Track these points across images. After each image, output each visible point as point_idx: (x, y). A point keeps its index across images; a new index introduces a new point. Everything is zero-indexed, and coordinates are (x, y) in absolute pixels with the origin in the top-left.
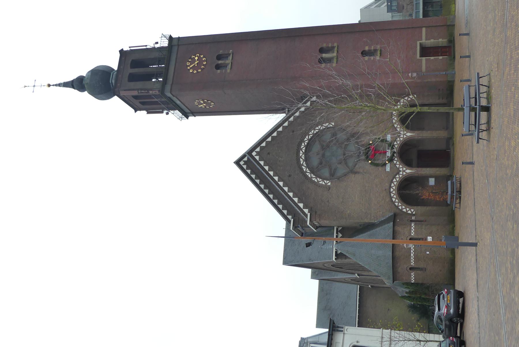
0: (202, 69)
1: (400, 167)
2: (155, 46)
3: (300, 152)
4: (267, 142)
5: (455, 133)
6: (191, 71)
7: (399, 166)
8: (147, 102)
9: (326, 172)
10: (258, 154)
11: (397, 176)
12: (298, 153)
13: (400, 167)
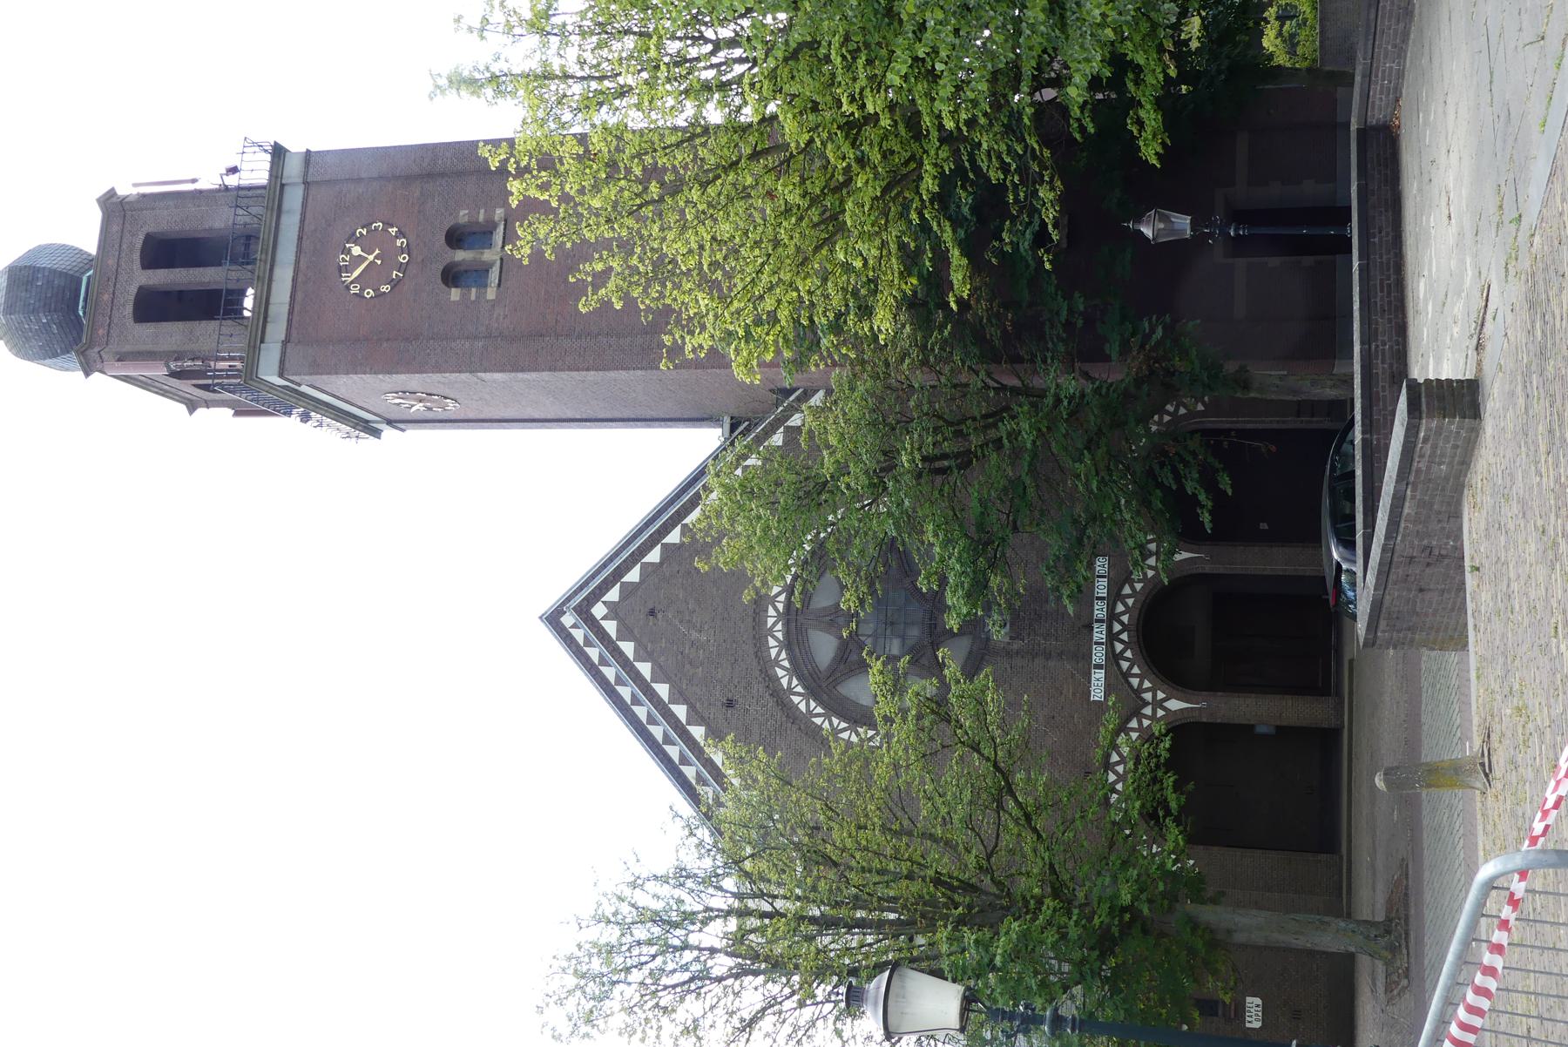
0: (395, 284)
1: (1144, 687)
2: (226, 183)
3: (767, 611)
4: (645, 566)
5: (1427, 839)
6: (354, 290)
10: (614, 611)
13: (1144, 687)
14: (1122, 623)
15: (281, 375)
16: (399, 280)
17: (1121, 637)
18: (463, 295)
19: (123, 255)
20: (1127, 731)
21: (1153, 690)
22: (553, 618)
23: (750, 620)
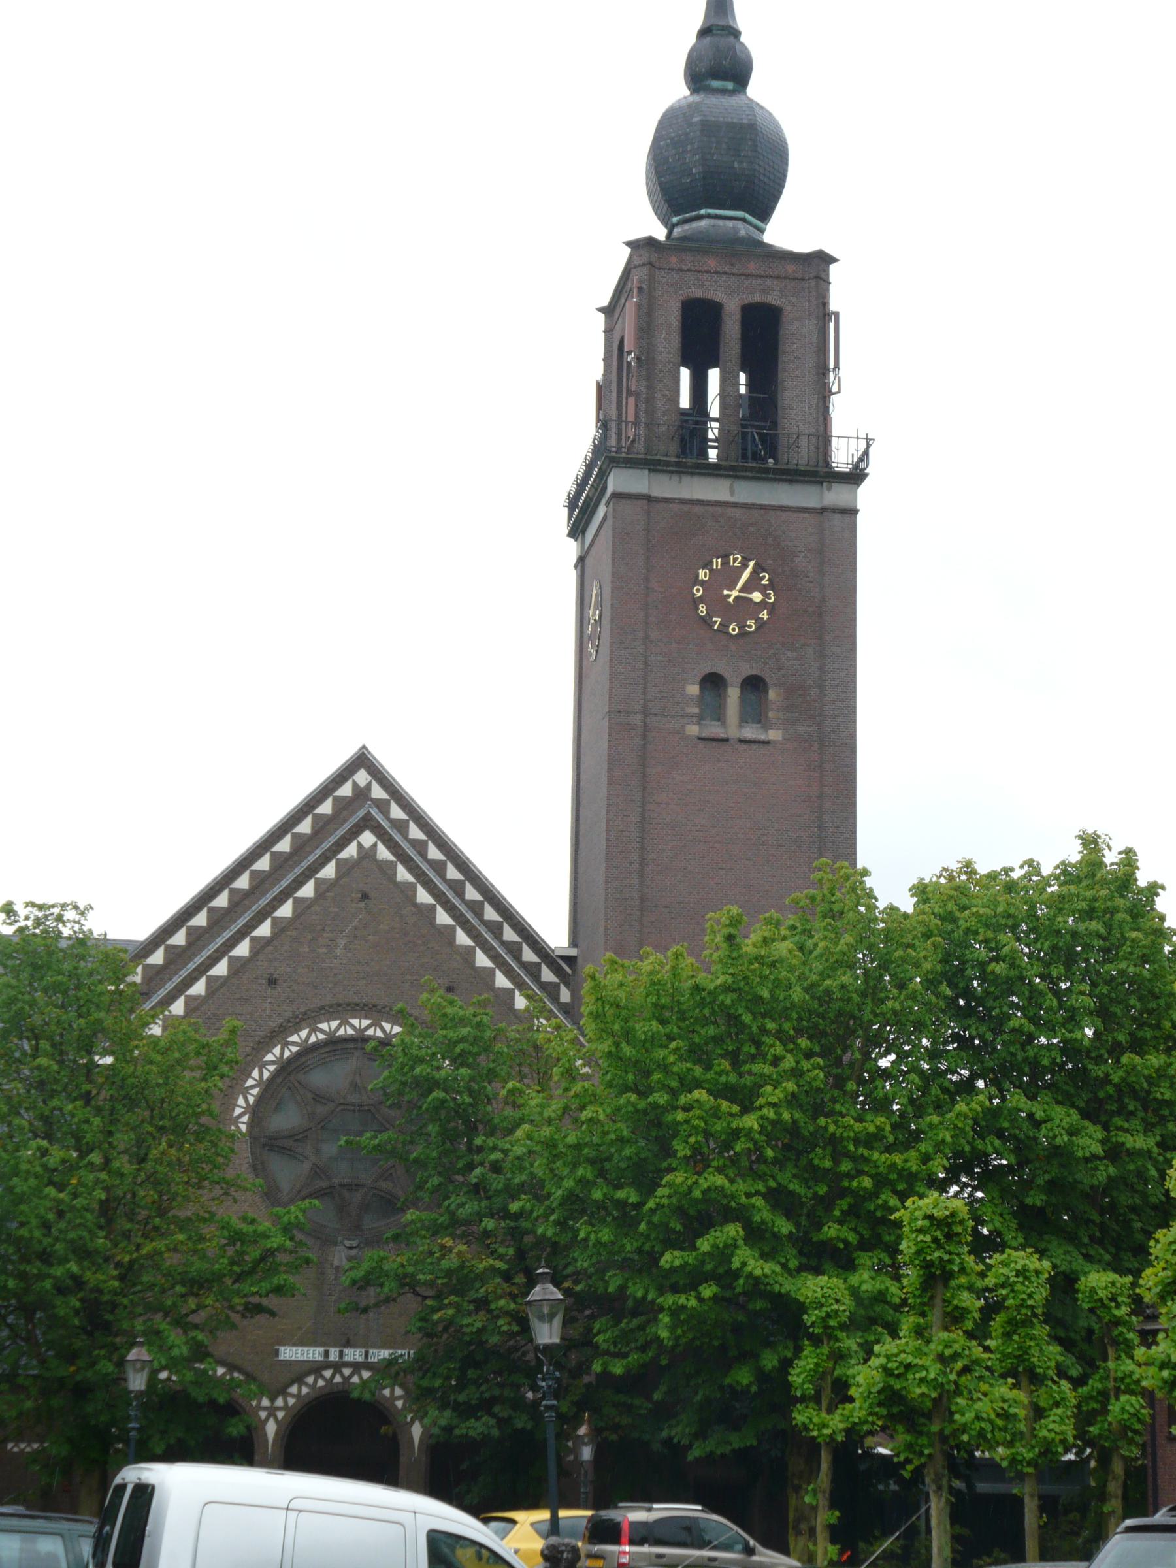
0: (706, 622)
7: (292, 1395)
9: (286, 1120)
10: (367, 855)
12: (362, 1009)
14: (351, 1376)
16: (710, 625)
18: (691, 698)
19: (760, 281)
21: (285, 1407)
23: (357, 1000)
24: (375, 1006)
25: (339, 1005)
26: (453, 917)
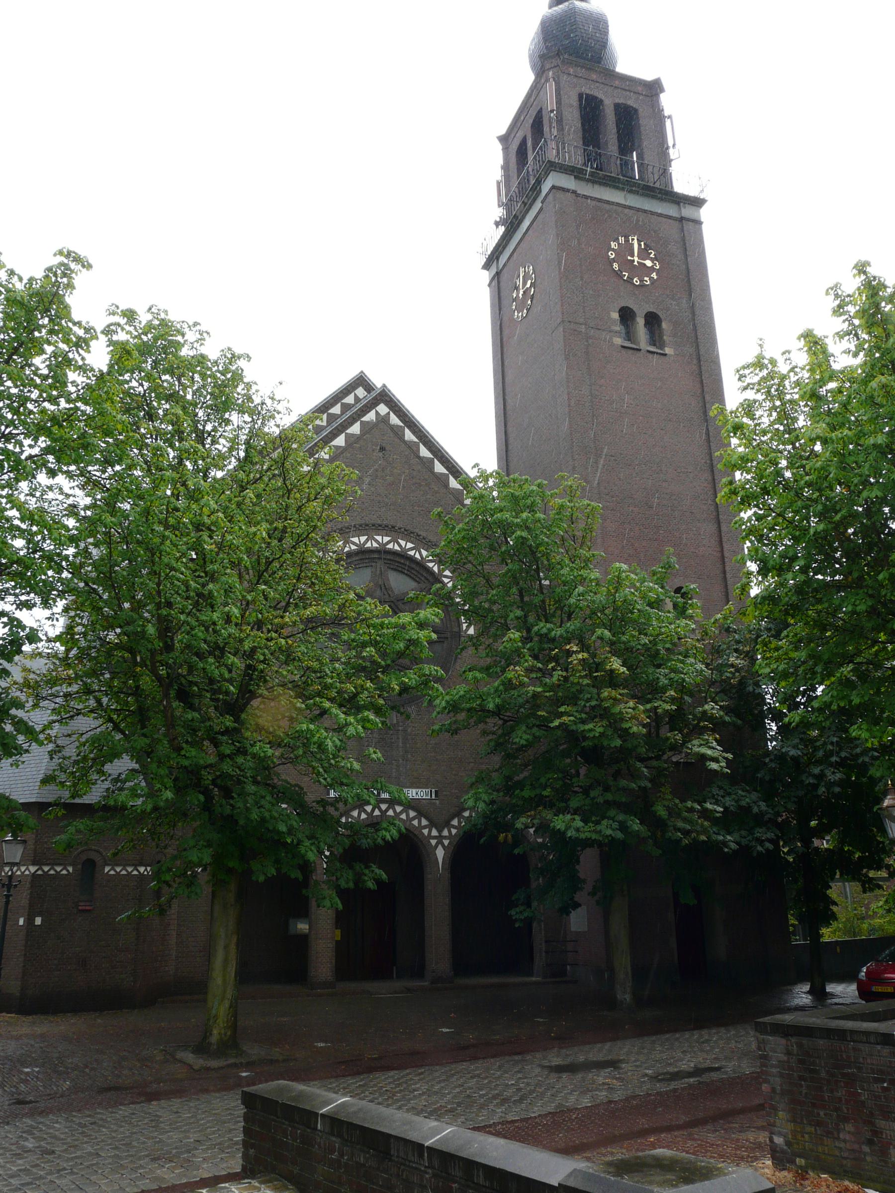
0: (618, 275)
3: (387, 536)
8: (853, 1032)
10: (385, 420)
11: (424, 822)
14: (387, 810)
15: (553, 187)
16: (622, 277)
17: (377, 810)
20: (405, 810)
22: (361, 381)
23: (379, 522)
24: (393, 527)
25: (367, 525)
26: (447, 468)
